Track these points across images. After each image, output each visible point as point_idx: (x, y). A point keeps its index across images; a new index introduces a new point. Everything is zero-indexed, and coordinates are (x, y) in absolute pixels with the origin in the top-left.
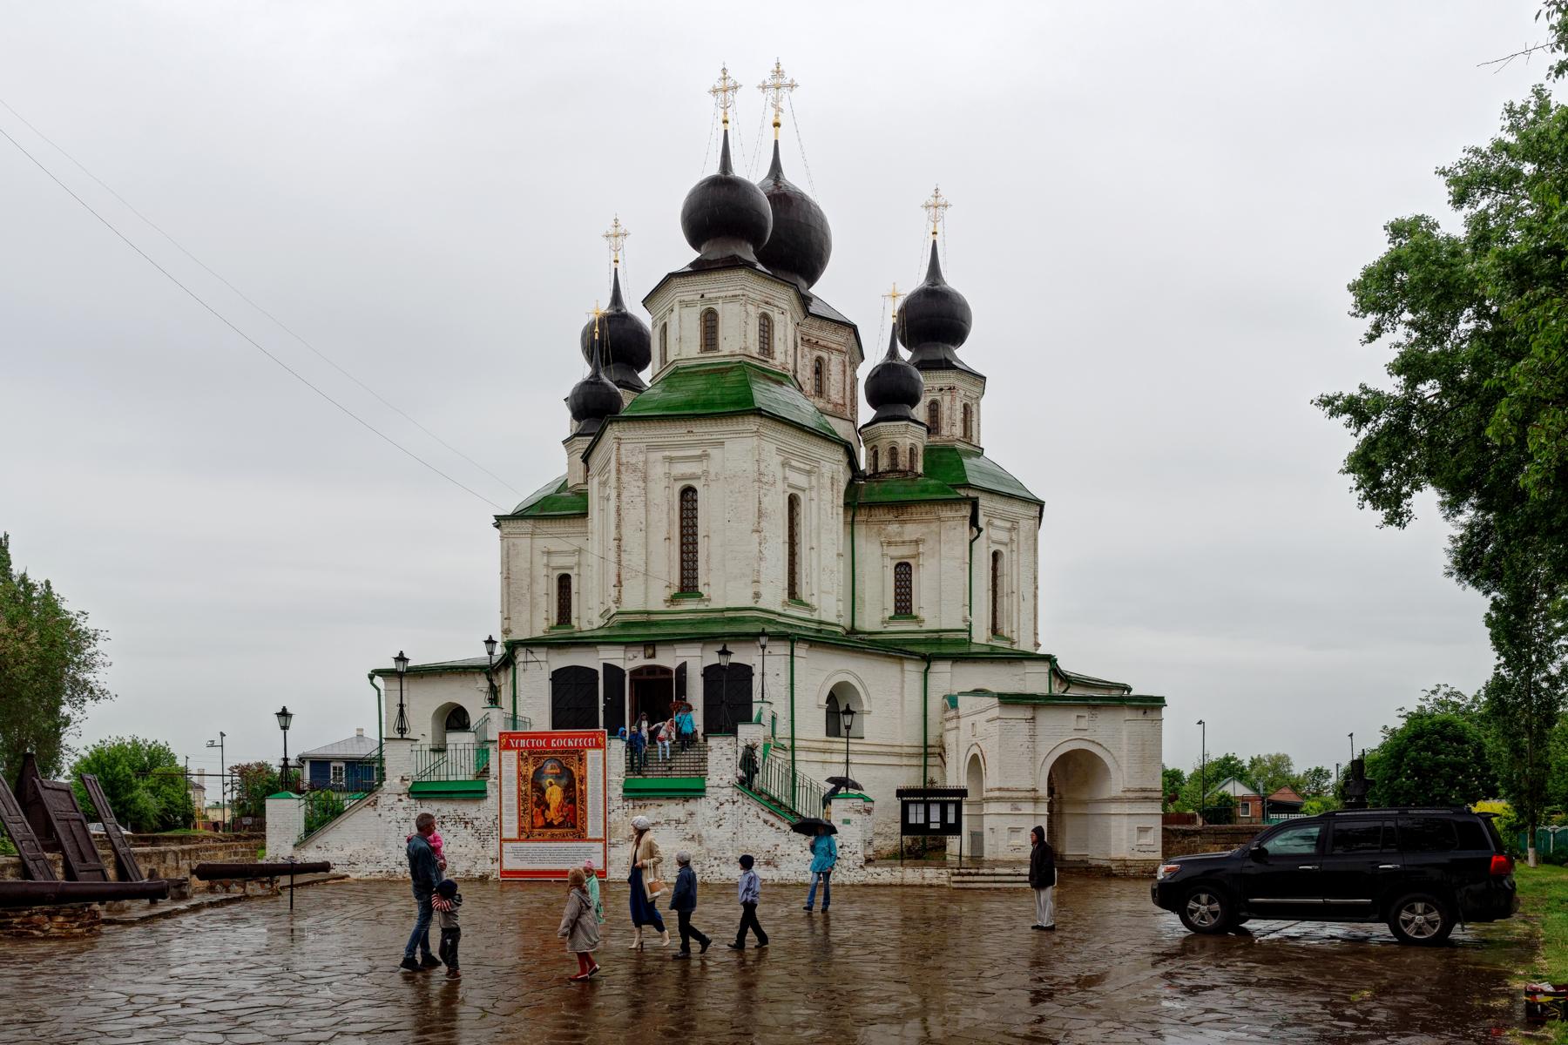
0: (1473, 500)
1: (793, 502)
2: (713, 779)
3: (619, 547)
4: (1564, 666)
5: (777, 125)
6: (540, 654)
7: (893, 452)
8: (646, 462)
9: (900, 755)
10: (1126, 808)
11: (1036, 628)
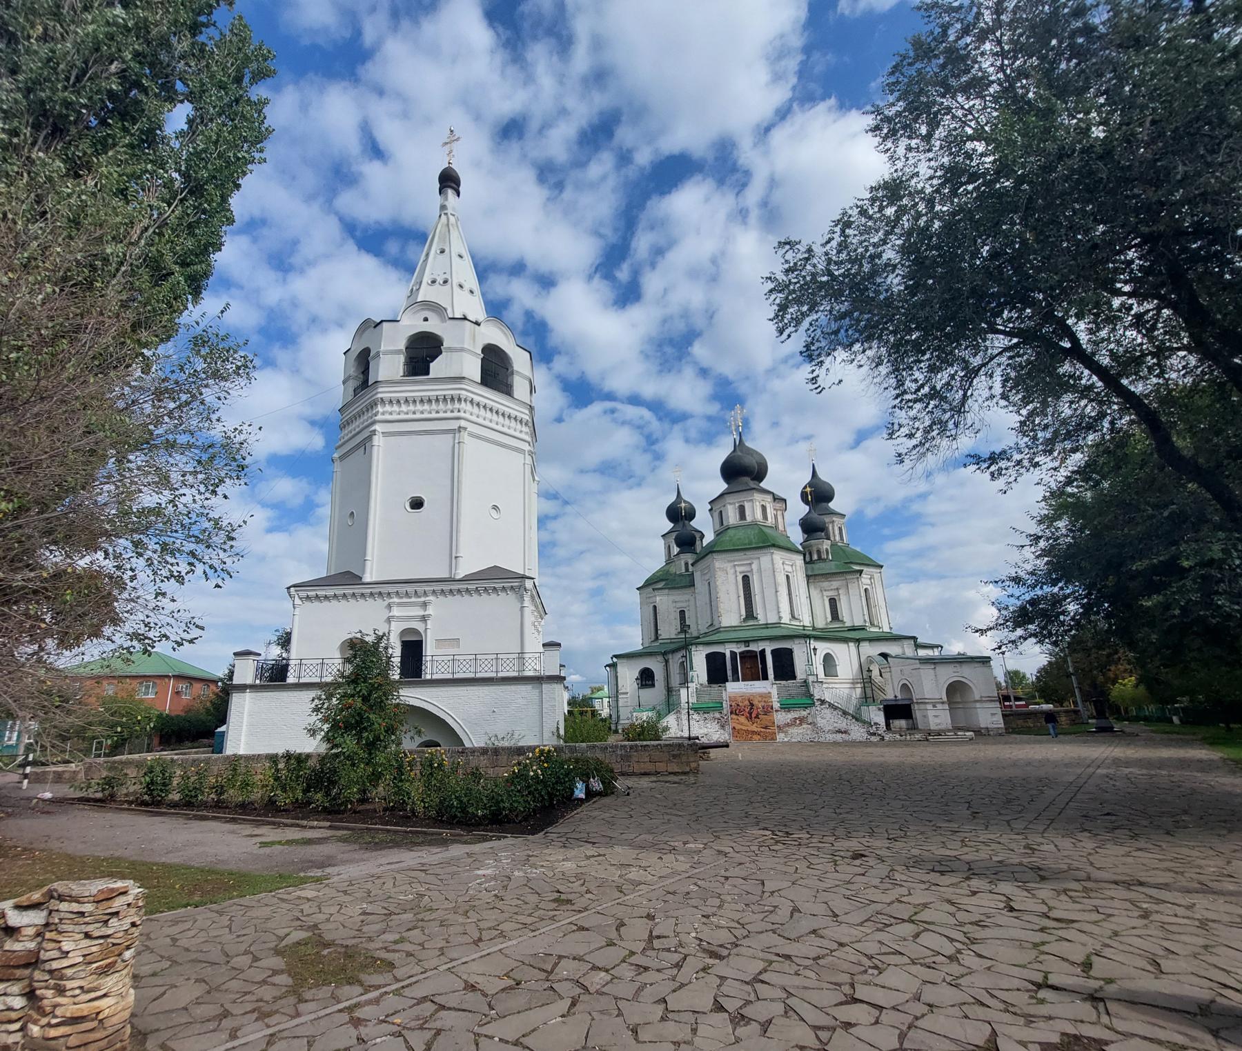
0: (895, 282)
1: (788, 577)
2: (764, 691)
4: (828, 61)
6: (700, 647)
7: (819, 552)
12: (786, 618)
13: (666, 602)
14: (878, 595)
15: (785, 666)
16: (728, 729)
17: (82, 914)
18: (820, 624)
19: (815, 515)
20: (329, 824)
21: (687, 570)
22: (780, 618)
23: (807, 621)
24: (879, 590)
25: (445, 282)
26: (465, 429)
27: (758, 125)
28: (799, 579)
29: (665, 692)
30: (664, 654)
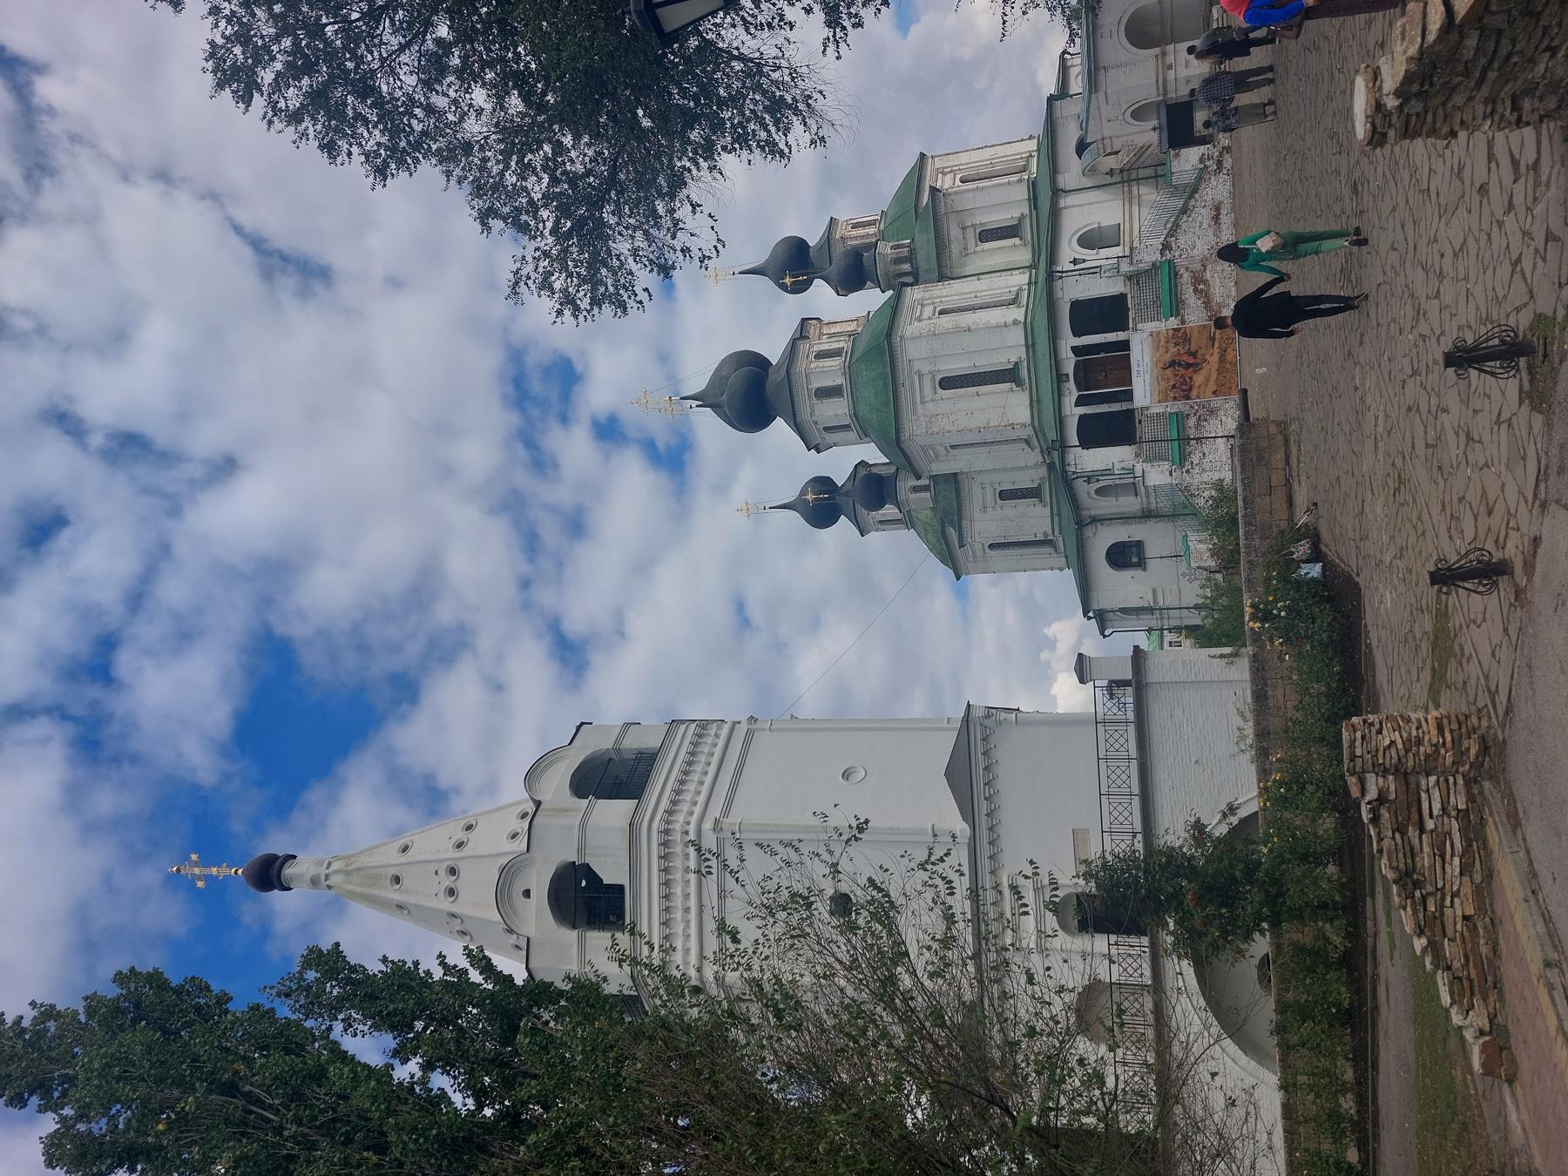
7: (898, 261)
12: (1017, 313)
14: (971, 160)
15: (1103, 314)
16: (1217, 402)
17: (1363, 738)
18: (1025, 256)
19: (833, 270)
20: (1368, 899)
21: (926, 488)
22: (1015, 322)
23: (1021, 279)
24: (964, 158)
25: (452, 871)
26: (717, 821)
27: (70, 399)
28: (949, 292)
29: (1151, 524)
30: (1081, 524)
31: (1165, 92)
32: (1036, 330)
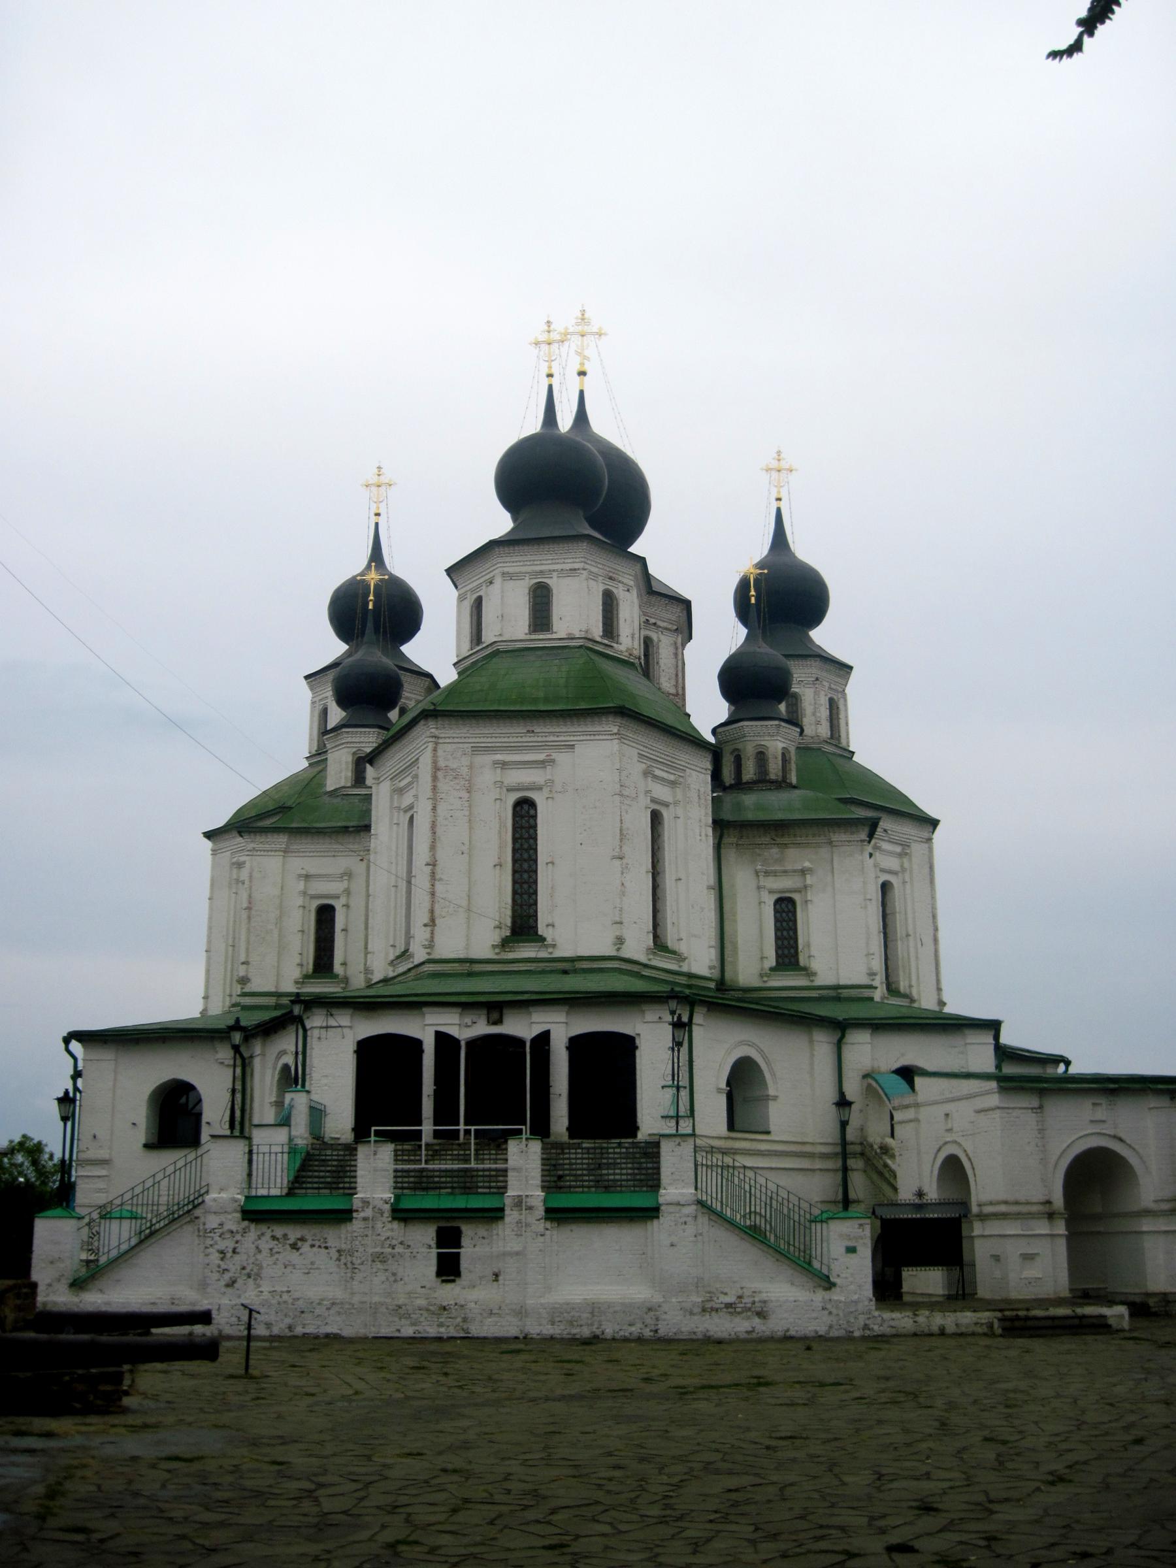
3: (433, 874)
5: (582, 373)
6: (343, 1018)
8: (471, 767)
9: (811, 1156)
10: (1162, 1225)
11: (938, 981)
13: (287, 876)
22: (620, 941)
31: (983, 1217)
32: (597, 977)
